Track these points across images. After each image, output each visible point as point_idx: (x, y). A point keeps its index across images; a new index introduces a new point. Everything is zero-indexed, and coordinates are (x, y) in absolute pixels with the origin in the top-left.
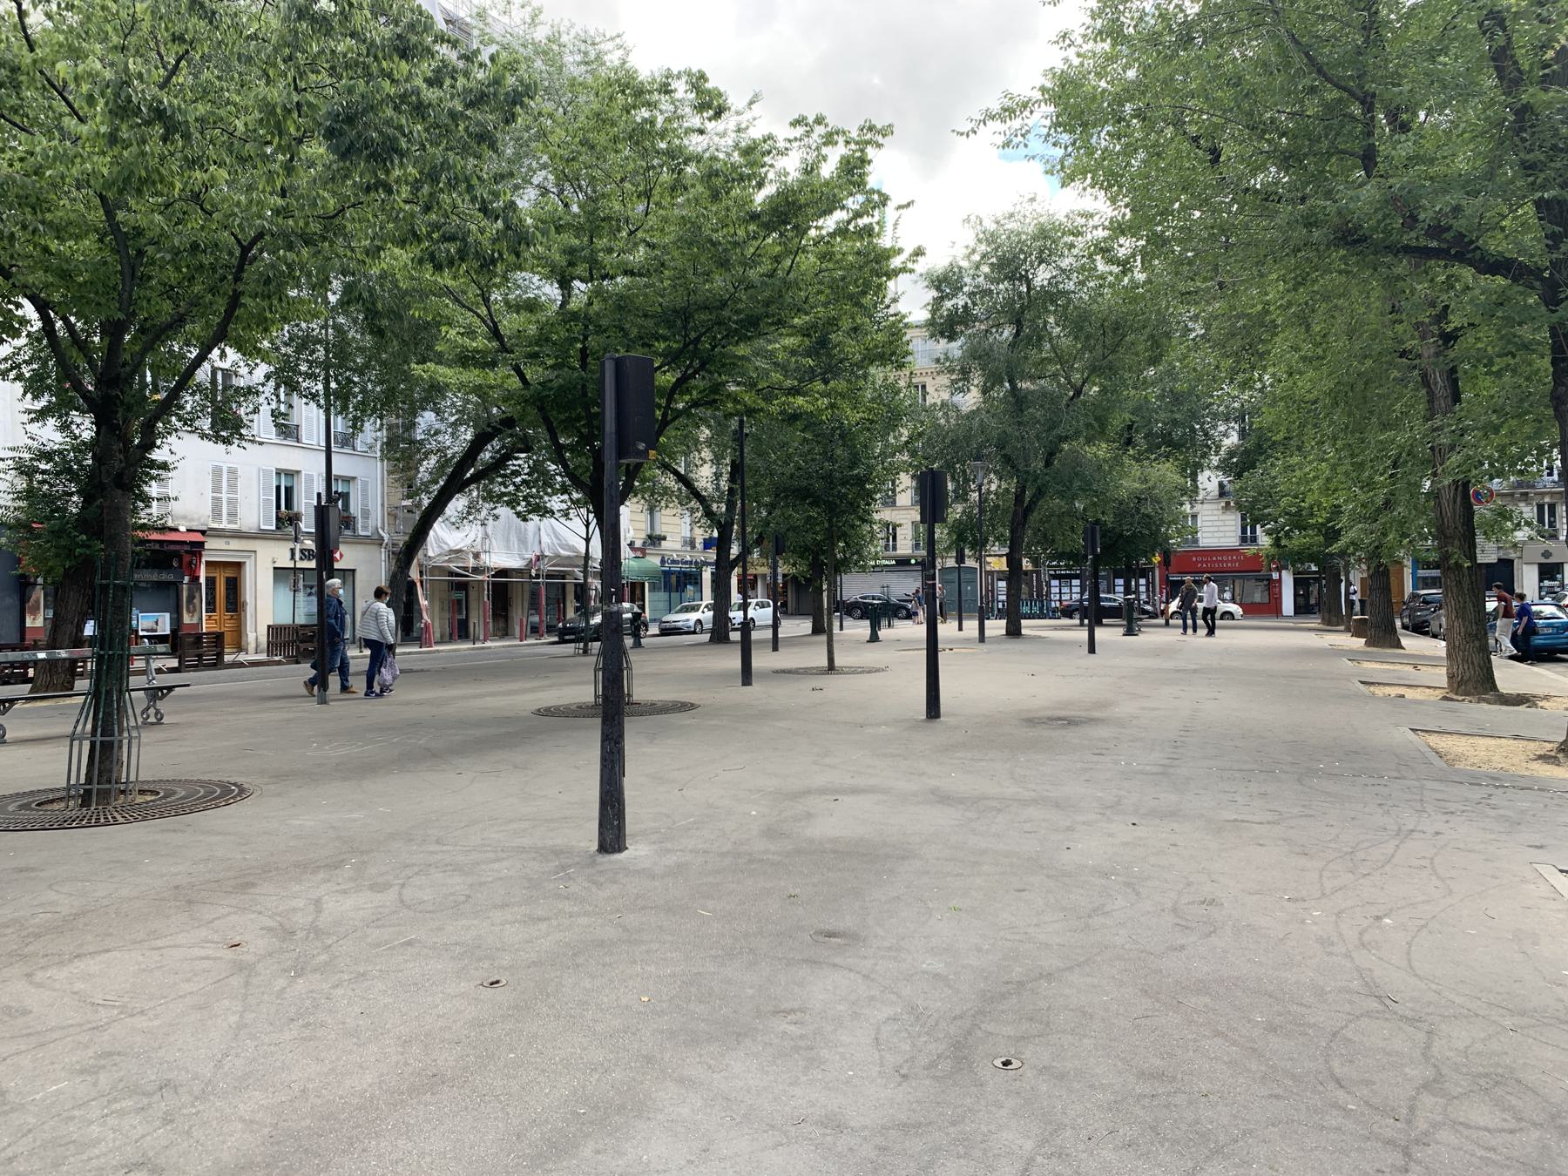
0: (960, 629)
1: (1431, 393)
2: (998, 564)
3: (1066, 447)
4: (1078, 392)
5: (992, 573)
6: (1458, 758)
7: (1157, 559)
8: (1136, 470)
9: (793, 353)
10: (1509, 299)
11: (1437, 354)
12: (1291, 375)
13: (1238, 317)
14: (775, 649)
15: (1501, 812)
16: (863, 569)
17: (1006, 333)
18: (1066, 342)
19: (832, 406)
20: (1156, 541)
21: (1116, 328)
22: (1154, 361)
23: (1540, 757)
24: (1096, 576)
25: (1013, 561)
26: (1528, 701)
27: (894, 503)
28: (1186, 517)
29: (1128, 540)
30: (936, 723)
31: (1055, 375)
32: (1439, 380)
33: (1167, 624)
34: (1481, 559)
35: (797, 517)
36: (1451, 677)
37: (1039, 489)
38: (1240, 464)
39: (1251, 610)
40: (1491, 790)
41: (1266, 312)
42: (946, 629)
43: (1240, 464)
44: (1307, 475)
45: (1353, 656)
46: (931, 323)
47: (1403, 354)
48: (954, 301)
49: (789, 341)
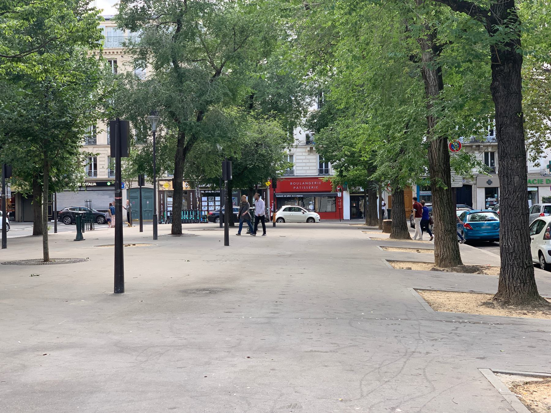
0: (141, 230)
1: (427, 83)
2: (168, 186)
3: (211, 108)
4: (218, 72)
5: (163, 192)
6: (440, 305)
7: (268, 183)
8: (255, 125)
9: (17, 31)
10: (469, 28)
11: (431, 59)
12: (347, 68)
13: (316, 28)
14: (4, 246)
15: (463, 338)
16: (73, 189)
17: (171, 29)
18: (210, 38)
19: (46, 71)
20: (269, 173)
21: (243, 31)
22: (266, 55)
23: (484, 304)
24: (230, 194)
25: (177, 185)
26: (478, 270)
27: (95, 142)
28: (286, 156)
29: (251, 171)
30: (121, 296)
31: (203, 60)
32: (431, 75)
33: (274, 226)
34: (453, 185)
35: (21, 151)
36: (437, 256)
37: (193, 135)
38: (319, 123)
39: (325, 216)
40: (457, 325)
41: (334, 26)
42: (128, 231)
43: (319, 123)
44: (358, 130)
45: (383, 245)
46: (119, 18)
47: (412, 58)
48: (135, 4)
49: (14, 23)
